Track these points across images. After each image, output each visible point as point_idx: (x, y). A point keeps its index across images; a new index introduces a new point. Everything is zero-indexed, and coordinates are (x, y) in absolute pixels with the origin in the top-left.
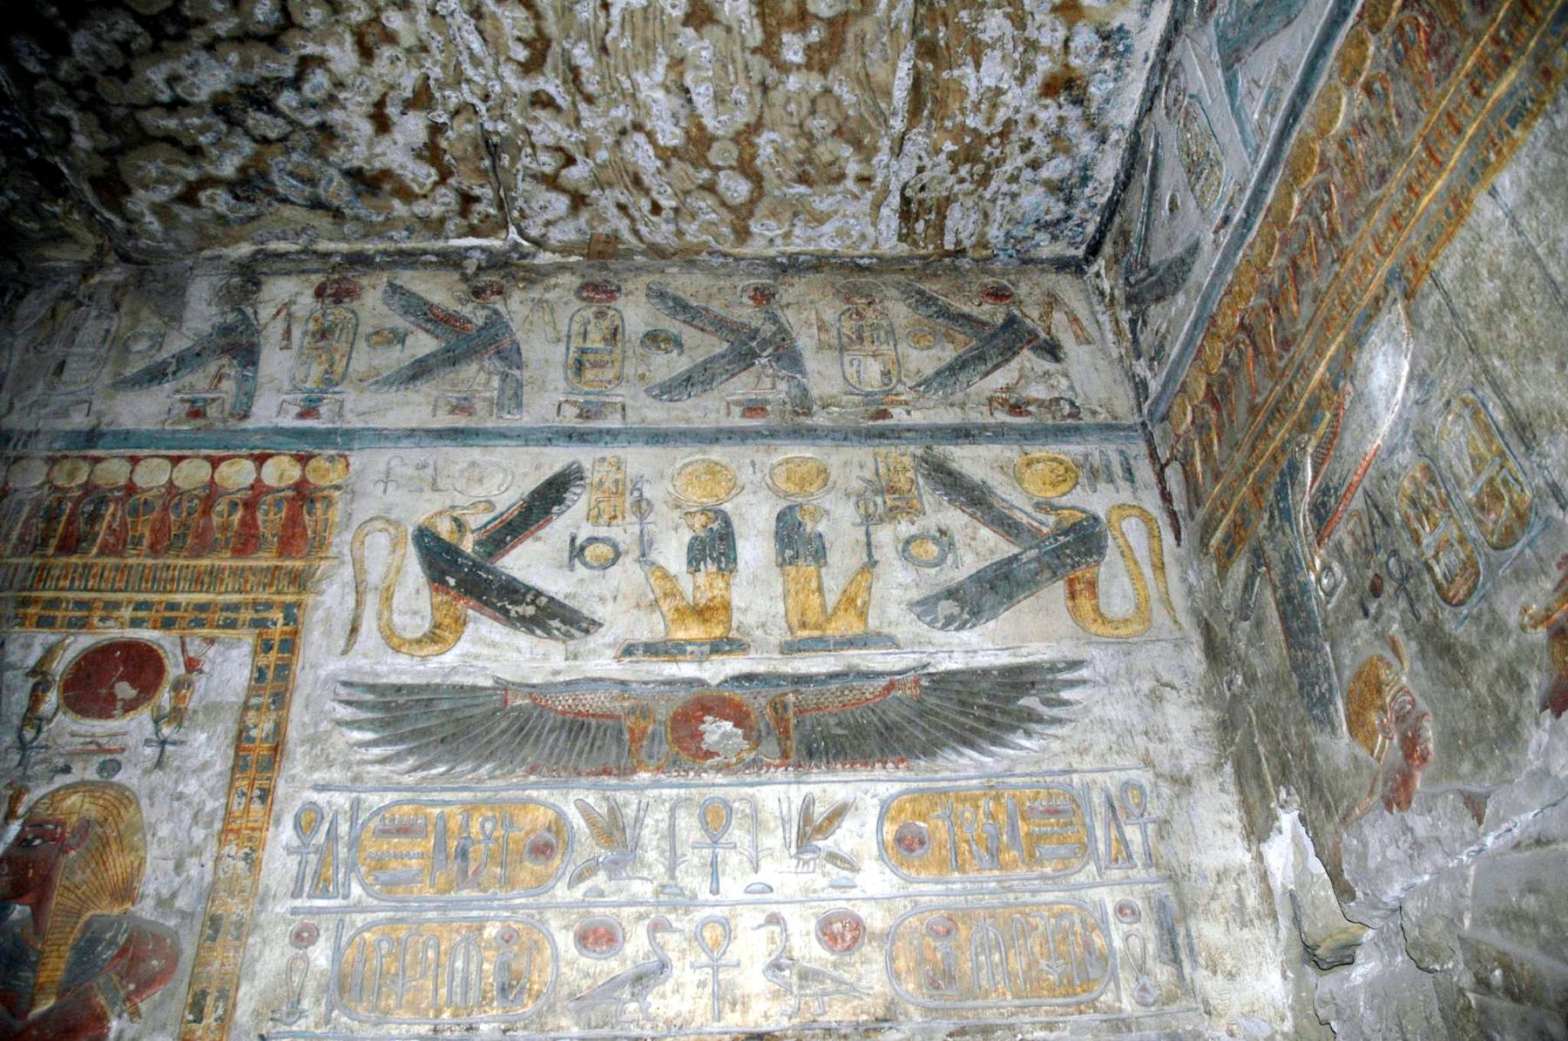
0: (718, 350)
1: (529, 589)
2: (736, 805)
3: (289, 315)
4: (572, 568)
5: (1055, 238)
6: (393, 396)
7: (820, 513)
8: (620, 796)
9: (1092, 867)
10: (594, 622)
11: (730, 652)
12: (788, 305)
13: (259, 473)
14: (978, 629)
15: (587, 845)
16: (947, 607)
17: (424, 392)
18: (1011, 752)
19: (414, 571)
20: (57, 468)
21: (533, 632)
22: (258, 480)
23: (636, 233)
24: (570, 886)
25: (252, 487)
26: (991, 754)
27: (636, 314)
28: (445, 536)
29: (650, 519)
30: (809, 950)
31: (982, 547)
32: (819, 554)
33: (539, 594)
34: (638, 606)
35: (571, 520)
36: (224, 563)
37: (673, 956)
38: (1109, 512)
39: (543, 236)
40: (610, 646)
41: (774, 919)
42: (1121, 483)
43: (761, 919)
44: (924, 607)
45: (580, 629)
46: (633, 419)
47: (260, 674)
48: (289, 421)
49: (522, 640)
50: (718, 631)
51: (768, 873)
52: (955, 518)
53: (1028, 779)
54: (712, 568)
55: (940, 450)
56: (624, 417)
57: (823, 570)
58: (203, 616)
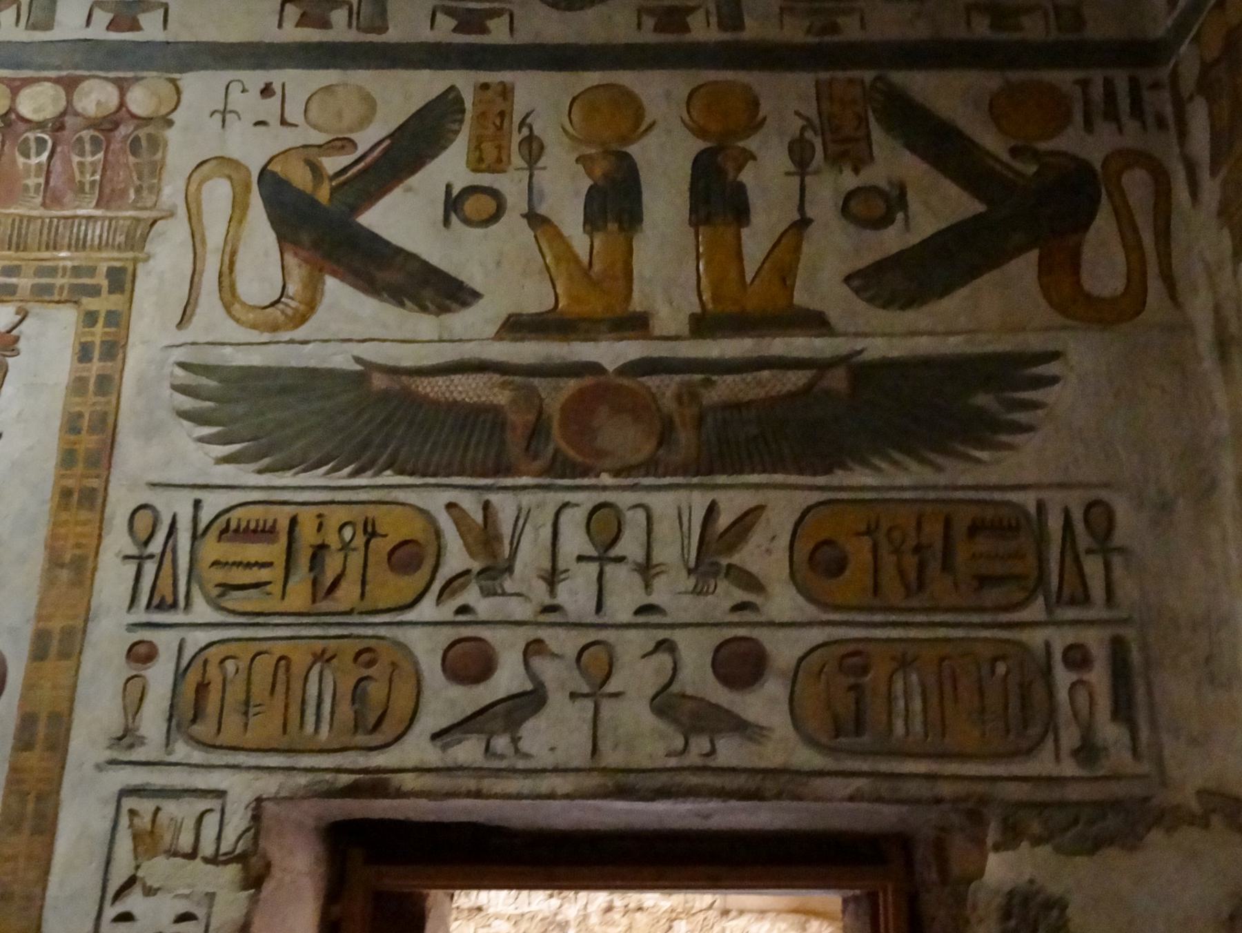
8: (495, 498)
9: (1040, 600)
13: (13, 100)
15: (456, 558)
19: (260, 232)
20: (163, 111)
22: (12, 109)
30: (697, 676)
31: (937, 205)
32: (740, 212)
35: (451, 166)
37: (550, 685)
38: (1106, 162)
43: (650, 646)
46: (524, 36)
48: (99, 31)
54: (613, 226)
55: (898, 77)
56: (512, 29)
58: (14, 280)
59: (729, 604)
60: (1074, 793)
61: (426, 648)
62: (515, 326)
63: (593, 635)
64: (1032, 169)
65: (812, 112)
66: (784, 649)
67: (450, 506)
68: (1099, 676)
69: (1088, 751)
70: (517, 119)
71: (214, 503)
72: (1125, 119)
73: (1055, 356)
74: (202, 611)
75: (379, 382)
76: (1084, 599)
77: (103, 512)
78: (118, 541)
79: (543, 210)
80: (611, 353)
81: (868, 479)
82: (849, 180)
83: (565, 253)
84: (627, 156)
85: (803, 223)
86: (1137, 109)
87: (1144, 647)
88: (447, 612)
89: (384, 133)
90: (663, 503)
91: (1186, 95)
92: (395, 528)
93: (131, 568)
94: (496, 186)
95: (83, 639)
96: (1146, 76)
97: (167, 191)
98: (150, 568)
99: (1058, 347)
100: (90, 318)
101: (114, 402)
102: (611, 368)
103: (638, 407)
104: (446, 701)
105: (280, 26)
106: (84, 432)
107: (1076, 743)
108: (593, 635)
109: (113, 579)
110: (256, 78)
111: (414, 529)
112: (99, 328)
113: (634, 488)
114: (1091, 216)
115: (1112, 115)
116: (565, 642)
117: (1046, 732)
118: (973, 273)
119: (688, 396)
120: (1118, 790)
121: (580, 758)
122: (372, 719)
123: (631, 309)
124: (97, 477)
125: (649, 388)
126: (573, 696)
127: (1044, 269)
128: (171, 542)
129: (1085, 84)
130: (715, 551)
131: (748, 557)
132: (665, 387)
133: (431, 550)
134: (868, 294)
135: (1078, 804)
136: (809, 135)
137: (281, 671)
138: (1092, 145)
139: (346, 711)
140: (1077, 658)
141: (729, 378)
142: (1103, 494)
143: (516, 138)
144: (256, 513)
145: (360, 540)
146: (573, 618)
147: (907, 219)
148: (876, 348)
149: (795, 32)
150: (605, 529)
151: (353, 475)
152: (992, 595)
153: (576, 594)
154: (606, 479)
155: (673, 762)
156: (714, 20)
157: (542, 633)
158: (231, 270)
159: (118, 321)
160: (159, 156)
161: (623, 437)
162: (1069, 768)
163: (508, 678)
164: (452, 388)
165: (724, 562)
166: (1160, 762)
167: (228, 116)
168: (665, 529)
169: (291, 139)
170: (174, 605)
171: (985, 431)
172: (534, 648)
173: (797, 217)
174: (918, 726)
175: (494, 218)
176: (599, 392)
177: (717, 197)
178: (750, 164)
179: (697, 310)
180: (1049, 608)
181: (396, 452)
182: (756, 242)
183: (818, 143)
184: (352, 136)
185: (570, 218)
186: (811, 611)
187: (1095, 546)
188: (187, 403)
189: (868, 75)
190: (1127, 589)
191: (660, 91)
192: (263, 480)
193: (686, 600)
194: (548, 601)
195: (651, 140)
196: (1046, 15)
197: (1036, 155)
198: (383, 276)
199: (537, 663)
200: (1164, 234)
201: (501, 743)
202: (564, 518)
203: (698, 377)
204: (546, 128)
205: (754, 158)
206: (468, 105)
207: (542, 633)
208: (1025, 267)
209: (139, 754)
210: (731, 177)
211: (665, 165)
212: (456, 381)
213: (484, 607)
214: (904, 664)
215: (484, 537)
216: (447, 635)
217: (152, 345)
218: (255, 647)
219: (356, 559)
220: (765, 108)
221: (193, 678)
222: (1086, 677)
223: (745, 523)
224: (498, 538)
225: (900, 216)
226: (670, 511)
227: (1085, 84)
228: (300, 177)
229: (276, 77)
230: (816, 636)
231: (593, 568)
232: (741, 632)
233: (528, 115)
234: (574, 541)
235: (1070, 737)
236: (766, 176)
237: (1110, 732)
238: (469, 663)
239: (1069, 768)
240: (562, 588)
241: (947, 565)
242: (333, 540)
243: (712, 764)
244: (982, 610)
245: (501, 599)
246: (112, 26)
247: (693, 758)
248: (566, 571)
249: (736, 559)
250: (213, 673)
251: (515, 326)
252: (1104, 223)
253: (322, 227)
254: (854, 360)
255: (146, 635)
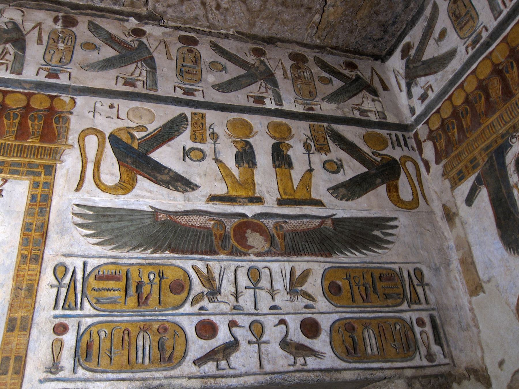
0: (242, 73)
1: (166, 168)
2: (263, 270)
3: (40, 29)
4: (184, 159)
5: (375, 46)
6: (92, 74)
7: (289, 147)
9: (406, 303)
10: (196, 186)
11: (256, 202)
12: (270, 59)
14: (354, 201)
15: (198, 287)
16: (342, 191)
17: (113, 73)
18: (371, 253)
21: (169, 188)
23: (207, 17)
24: (192, 305)
25: (24, 108)
26: (364, 254)
27: (206, 53)
28: (125, 140)
29: (218, 142)
30: (296, 335)
31: (353, 169)
32: (290, 165)
33: (170, 170)
34: (215, 179)
35: (184, 140)
36: (11, 143)
39: (165, 12)
40: (202, 196)
41: (282, 322)
42: (404, 147)
43: (277, 322)
44: (334, 190)
45: (190, 187)
46: (208, 99)
47: (33, 198)
48: (42, 78)
49: (164, 190)
50: (251, 194)
51: (278, 302)
52: (343, 155)
53: (378, 265)
54: (246, 166)
55: (335, 126)
57: (292, 171)
59: (303, 305)
60: (428, 371)
61: (189, 325)
62: (213, 198)
63: (254, 318)
64: (379, 159)
65: (309, 135)
66: (325, 322)
67: (193, 267)
68: (428, 329)
69: (430, 357)
70: (208, 126)
71: (93, 263)
72: (404, 147)
73: (395, 219)
74: (88, 309)
75: (162, 217)
76: (419, 302)
77: (41, 266)
78: (48, 277)
79: (220, 158)
80: (250, 210)
81: (345, 260)
82: (324, 157)
83: (230, 174)
84: (248, 143)
85: (311, 170)
86: (406, 145)
87: (440, 317)
88: (195, 309)
89: (158, 126)
90: (275, 267)
91: (422, 140)
92: (171, 275)
93: (55, 290)
94: (202, 148)
95: (32, 321)
96: (407, 135)
97: (70, 137)
98: (64, 291)
99: (396, 216)
100: (36, 185)
101: (47, 219)
102: (250, 215)
103: (262, 230)
104: (198, 347)
105: (116, 84)
106: (33, 231)
107: (426, 353)
108: (254, 318)
109: (46, 295)
110: (108, 101)
111: (180, 275)
112: (40, 190)
113: (264, 261)
114: (399, 175)
115: (400, 145)
116: (244, 321)
117: (416, 350)
118: (366, 191)
119: (277, 226)
120: (442, 369)
121: (255, 368)
122: (167, 356)
123: (256, 195)
124: (39, 250)
125: (264, 224)
126: (250, 343)
127: (389, 191)
128: (73, 278)
129: (390, 135)
130: (296, 284)
131: (307, 287)
132: (270, 223)
133: (188, 285)
134: (335, 195)
135: (431, 376)
136: (309, 141)
137: (126, 337)
138: (397, 154)
139: (156, 352)
140: (421, 322)
141: (292, 221)
142: (418, 266)
143: (208, 133)
144: (112, 268)
145: (157, 280)
146: (246, 311)
147: (344, 170)
148: (341, 214)
149: (300, 109)
150: (254, 276)
151: (153, 252)
152: (390, 302)
153: (246, 301)
154: (253, 257)
155: (291, 368)
156: (273, 102)
157: (236, 318)
158: (98, 170)
159: (50, 186)
160: (67, 125)
161: (255, 240)
162: (425, 363)
163: (223, 336)
164: (191, 220)
165: (300, 289)
166: (452, 358)
167: (96, 113)
168: (277, 276)
169: (121, 124)
170: (76, 308)
171: (377, 243)
172: (232, 324)
173: (309, 168)
174: (375, 350)
175: (203, 159)
176: (245, 225)
177: (281, 158)
178: (291, 149)
179: (279, 197)
180: (409, 306)
181: (170, 244)
182: (297, 174)
183: (312, 144)
184: (147, 126)
185: (231, 162)
186: (332, 308)
187: (419, 283)
188: (79, 220)
189: (325, 125)
190: (431, 297)
191: (258, 123)
192: (115, 253)
193: (288, 303)
194: (235, 304)
195: (256, 137)
196: (375, 113)
197: (380, 155)
198: (160, 177)
199: (234, 329)
200: (420, 183)
201: (223, 363)
202: (239, 272)
203: (282, 220)
204: (220, 130)
205: (292, 147)
206: (189, 119)
207: (236, 318)
208: (382, 189)
209: (61, 375)
210: (285, 153)
211: (262, 146)
212: (192, 218)
213: (210, 306)
214: (366, 326)
215: (208, 279)
216: (196, 319)
217: (65, 198)
218: (113, 325)
219: (156, 288)
220: (293, 131)
221: (86, 338)
222: (425, 329)
223: (306, 274)
224: (214, 279)
225: (342, 170)
226: (279, 268)
227: (390, 135)
228: (124, 137)
229: (116, 102)
230: (336, 317)
231: (252, 291)
232: (309, 316)
233: (212, 125)
234: (243, 281)
235: (423, 350)
236: (296, 152)
237: (436, 349)
238: (206, 330)
239: (425, 363)
240: (241, 299)
241: (375, 291)
242: (146, 280)
243: (305, 368)
244: (388, 306)
245: (218, 304)
246: (47, 76)
247: (298, 367)
248: (242, 292)
249: (303, 288)
250: (95, 337)
251: (213, 198)
252: (403, 177)
253: (136, 158)
254: (334, 217)
255: (63, 320)
